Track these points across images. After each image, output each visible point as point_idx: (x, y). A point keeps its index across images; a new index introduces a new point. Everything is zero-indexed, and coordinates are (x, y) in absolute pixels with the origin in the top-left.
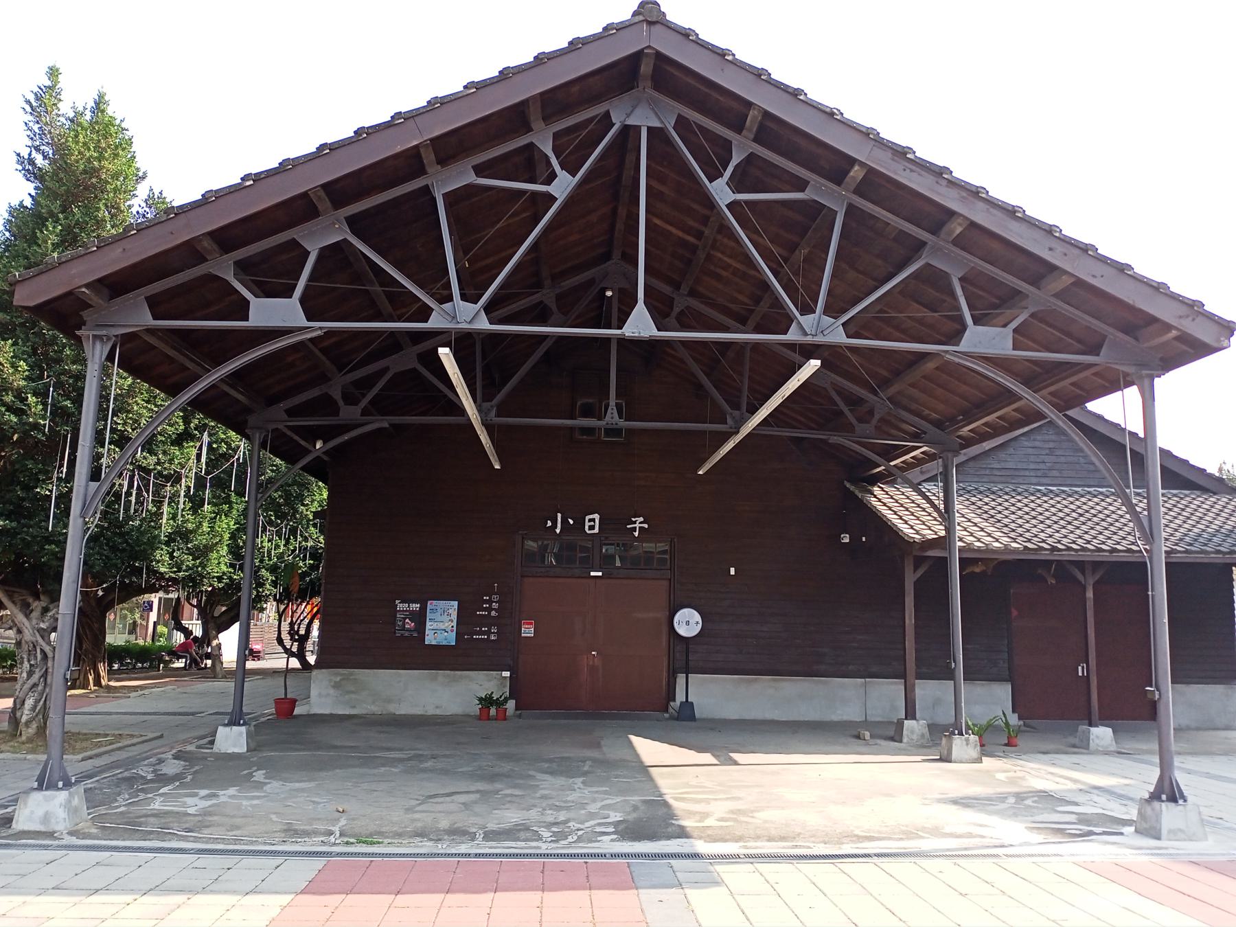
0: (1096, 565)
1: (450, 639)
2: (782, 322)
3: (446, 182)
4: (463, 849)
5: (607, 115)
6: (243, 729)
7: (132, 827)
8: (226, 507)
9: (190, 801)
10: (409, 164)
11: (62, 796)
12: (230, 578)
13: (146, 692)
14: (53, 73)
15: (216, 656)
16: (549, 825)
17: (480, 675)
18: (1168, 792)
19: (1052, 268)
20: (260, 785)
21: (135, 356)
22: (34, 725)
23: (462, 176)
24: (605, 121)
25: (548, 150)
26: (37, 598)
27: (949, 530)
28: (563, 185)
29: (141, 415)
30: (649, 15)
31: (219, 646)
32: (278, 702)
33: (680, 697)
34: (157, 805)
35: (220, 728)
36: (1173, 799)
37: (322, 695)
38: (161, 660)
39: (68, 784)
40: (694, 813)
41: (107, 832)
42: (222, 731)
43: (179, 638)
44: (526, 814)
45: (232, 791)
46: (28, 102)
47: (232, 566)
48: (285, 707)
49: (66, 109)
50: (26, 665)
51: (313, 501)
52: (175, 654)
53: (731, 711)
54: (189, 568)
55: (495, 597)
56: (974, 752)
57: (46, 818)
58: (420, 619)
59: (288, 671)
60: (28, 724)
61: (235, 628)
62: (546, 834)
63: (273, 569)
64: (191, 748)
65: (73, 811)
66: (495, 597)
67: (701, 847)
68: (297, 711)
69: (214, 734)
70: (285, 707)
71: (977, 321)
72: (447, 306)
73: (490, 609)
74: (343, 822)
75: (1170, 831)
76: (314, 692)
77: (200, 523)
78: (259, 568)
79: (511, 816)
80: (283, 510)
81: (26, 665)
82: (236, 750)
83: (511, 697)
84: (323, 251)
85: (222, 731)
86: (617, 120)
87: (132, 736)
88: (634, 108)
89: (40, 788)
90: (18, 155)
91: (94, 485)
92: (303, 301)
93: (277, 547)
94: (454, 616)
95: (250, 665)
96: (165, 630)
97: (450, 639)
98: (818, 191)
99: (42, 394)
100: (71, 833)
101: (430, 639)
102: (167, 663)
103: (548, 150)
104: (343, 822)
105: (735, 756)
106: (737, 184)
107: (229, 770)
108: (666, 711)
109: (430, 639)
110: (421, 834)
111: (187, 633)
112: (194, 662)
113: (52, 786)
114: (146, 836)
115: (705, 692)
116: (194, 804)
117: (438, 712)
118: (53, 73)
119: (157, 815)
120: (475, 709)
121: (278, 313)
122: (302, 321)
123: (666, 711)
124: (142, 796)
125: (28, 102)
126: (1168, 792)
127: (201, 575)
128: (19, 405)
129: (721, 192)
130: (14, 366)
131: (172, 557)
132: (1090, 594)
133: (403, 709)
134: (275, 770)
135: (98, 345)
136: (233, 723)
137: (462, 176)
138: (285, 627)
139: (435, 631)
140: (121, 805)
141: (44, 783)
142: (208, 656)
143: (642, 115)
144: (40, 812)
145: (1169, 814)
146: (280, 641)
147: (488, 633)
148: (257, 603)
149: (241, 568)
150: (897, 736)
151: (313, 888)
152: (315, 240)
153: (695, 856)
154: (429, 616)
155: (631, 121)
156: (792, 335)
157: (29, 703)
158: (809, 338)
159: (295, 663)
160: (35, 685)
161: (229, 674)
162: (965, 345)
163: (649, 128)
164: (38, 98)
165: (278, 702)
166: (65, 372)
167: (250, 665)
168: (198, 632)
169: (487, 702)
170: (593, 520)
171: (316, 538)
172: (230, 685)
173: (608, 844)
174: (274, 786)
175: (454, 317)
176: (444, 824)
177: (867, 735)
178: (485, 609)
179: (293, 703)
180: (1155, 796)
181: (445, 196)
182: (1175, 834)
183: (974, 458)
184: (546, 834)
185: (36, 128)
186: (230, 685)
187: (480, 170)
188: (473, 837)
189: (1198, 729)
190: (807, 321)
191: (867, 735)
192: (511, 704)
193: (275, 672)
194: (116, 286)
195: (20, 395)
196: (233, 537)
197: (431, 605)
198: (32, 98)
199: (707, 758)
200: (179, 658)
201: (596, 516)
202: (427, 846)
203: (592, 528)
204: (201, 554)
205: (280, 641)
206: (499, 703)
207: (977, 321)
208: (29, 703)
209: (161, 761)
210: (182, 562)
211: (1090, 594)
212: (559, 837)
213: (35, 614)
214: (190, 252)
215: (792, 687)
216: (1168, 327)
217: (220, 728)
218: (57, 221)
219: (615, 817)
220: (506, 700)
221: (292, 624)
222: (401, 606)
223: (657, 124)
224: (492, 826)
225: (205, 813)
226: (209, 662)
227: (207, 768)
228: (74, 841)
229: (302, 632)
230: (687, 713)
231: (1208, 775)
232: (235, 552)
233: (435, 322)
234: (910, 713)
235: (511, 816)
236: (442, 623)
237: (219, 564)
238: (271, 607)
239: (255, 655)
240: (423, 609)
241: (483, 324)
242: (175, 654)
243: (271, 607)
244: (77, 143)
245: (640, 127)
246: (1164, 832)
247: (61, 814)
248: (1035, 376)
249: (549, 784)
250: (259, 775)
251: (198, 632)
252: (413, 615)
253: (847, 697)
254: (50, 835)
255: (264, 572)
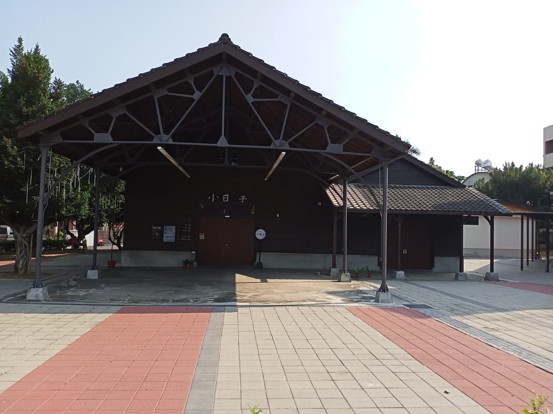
0: (403, 215)
1: (173, 240)
2: (269, 142)
3: (158, 94)
4: (165, 304)
5: (212, 72)
6: (97, 271)
7: (63, 299)
8: (86, 187)
9: (80, 292)
10: (146, 89)
11: (41, 289)
12: (89, 215)
13: (59, 258)
14: (20, 40)
15: (84, 244)
16: (193, 299)
17: (185, 253)
18: (384, 289)
19: (354, 127)
20: (103, 288)
21: (57, 150)
22: (23, 270)
23: (164, 92)
24: (212, 73)
25: (192, 84)
26: (22, 226)
27: (345, 203)
28: (197, 95)
29: (56, 163)
30: (225, 38)
31: (86, 241)
32: (109, 262)
33: (258, 261)
34: (70, 293)
35: (89, 271)
36: (384, 291)
37: (125, 261)
38: (62, 246)
39: (42, 286)
40: (241, 295)
41: (55, 300)
42: (89, 272)
43: (69, 237)
44: (187, 296)
45: (94, 290)
46: (12, 51)
47: (90, 210)
48: (112, 264)
49: (25, 52)
50: (19, 249)
51: (121, 186)
52: (68, 243)
53: (276, 266)
54: (73, 212)
55: (190, 225)
56: (348, 279)
57: (37, 296)
58: (161, 232)
59: (112, 251)
60: (21, 269)
61: (92, 234)
62: (191, 301)
63: (106, 211)
64: (79, 277)
65: (44, 294)
66: (190, 225)
67: (238, 304)
68: (116, 265)
69: (86, 273)
70: (112, 264)
71: (331, 143)
72: (158, 136)
73: (187, 229)
74: (129, 298)
75: (382, 300)
76: (122, 259)
77: (77, 195)
78: (100, 211)
79: (183, 297)
80: (110, 191)
81: (19, 249)
82: (94, 278)
83: (195, 261)
84: (118, 117)
85: (89, 272)
86: (215, 73)
87: (57, 274)
88: (221, 69)
89: (34, 287)
90: (8, 70)
91: (46, 194)
92: (111, 134)
93: (107, 202)
94: (174, 232)
95: (99, 248)
96: (63, 234)
97: (173, 240)
98: (282, 98)
99: (22, 157)
100: (45, 300)
101: (165, 240)
102: (64, 247)
103: (192, 84)
104: (129, 298)
105: (268, 280)
106: (254, 96)
107: (92, 284)
108: (253, 265)
109: (165, 240)
110: (153, 301)
111: (72, 235)
112: (76, 246)
113: (38, 287)
114: (68, 301)
115: (267, 259)
116: (82, 293)
117: (169, 266)
118: (20, 40)
119: (70, 296)
120: (182, 265)
121: (103, 138)
122: (111, 140)
123: (253, 265)
124: (64, 291)
125: (12, 51)
126: (384, 289)
127: (78, 215)
128: (14, 161)
129: (250, 98)
130: (13, 148)
131: (66, 208)
132: (400, 225)
133: (156, 265)
134: (108, 284)
135: (45, 149)
136: (93, 269)
137: (164, 92)
138: (112, 234)
139: (167, 237)
140: (58, 293)
141: (35, 286)
142: (81, 245)
143: (225, 71)
144: (35, 294)
145: (382, 296)
146: (110, 239)
147: (187, 238)
148: (101, 224)
149: (94, 211)
150: (329, 275)
151: (118, 312)
152: (115, 114)
153: (236, 306)
154: (165, 231)
155: (220, 74)
156: (272, 147)
157: (21, 262)
158: (277, 148)
159: (116, 247)
160: (23, 256)
161: (90, 252)
162: (327, 150)
163: (226, 76)
164: (15, 50)
165: (109, 262)
166: (29, 149)
167: (99, 248)
168: (76, 235)
169: (186, 262)
170: (226, 197)
171: (122, 199)
172: (91, 256)
173: (209, 303)
174: (107, 289)
175: (161, 140)
176: (161, 298)
177: (319, 273)
178: (185, 229)
179: (114, 263)
180: (380, 290)
181: (158, 99)
182: (383, 301)
183: (369, 174)
184: (191, 301)
185: (15, 61)
186: (91, 256)
187: (170, 90)
188: (169, 301)
189: (446, 273)
190: (277, 142)
191: (319, 273)
192: (195, 264)
193: (107, 251)
194: (51, 130)
195: (15, 157)
196: (90, 199)
197: (165, 227)
198: (13, 50)
199: (259, 280)
200: (69, 245)
201: (227, 195)
202: (154, 303)
203: (226, 199)
204: (78, 206)
205: (110, 239)
206: (191, 263)
207: (331, 143)
208: (21, 262)
209: (69, 281)
210: (71, 210)
211: (400, 225)
212: (195, 301)
213: (21, 232)
214: (74, 119)
215: (298, 257)
216: (389, 146)
217: (89, 271)
218: (24, 95)
219: (216, 296)
220: (193, 262)
221: (114, 233)
222: (154, 228)
223: (228, 75)
224: (176, 299)
225: (85, 295)
226: (82, 247)
227: (85, 283)
228: (44, 302)
229: (119, 235)
230: (260, 266)
231: (430, 289)
232: (91, 205)
233: (155, 141)
234: (334, 266)
235: (183, 297)
236: (169, 235)
237: (85, 210)
238: (106, 226)
239: (101, 244)
240: (163, 229)
241: (171, 142)
242: (68, 243)
243: (106, 226)
244: (30, 67)
245: (223, 76)
246: (380, 300)
247: (41, 295)
248: (352, 161)
249: (199, 288)
250: (103, 285)
251: (76, 235)
252: (158, 231)
253: (320, 260)
254: (39, 301)
255: (102, 212)
